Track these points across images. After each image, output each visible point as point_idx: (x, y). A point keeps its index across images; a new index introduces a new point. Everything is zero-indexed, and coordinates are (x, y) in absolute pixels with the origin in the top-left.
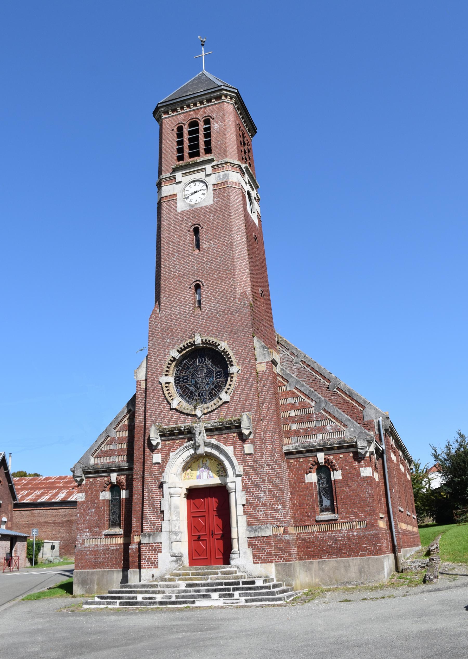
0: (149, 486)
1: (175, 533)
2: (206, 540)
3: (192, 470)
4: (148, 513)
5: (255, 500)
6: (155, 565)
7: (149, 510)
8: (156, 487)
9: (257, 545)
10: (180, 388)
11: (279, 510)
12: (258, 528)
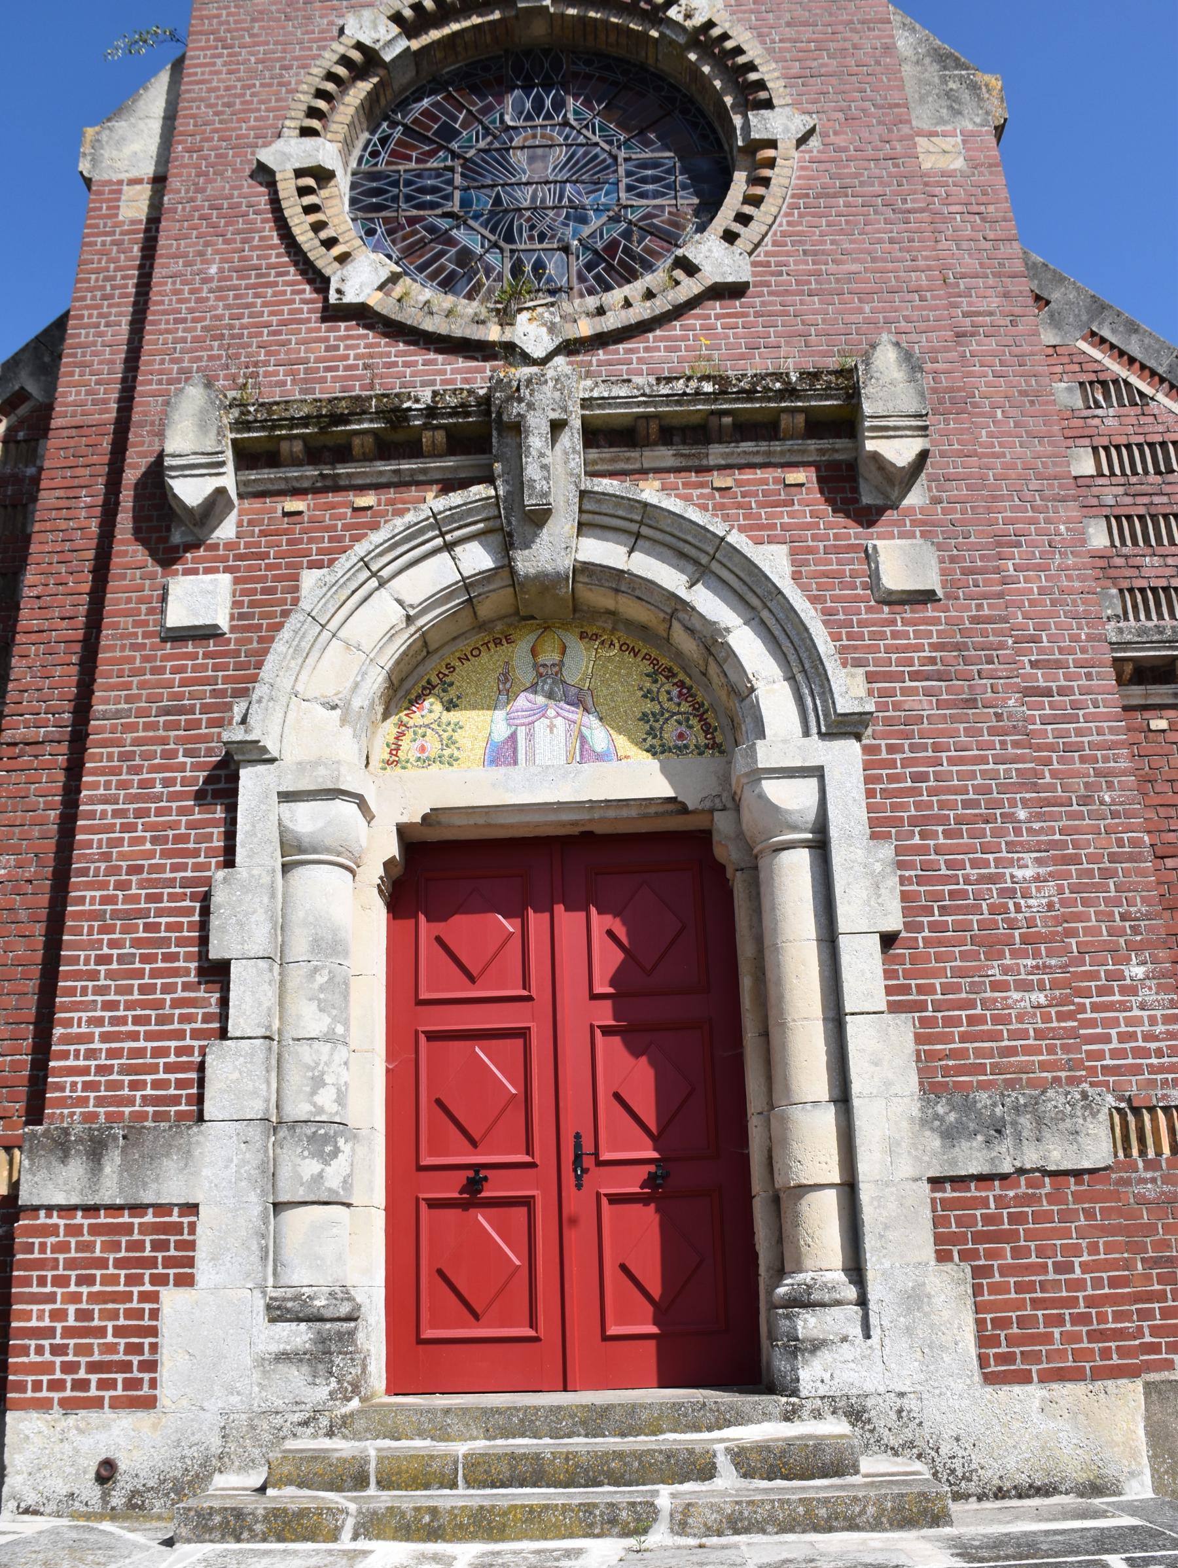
0: (123, 785)
1: (313, 1138)
2: (527, 1202)
3: (450, 706)
4: (93, 976)
5: (977, 910)
6: (131, 1384)
7: (104, 960)
8: (173, 797)
9: (1011, 1236)
10: (390, 232)
11: (1132, 990)
12: (1017, 1109)
